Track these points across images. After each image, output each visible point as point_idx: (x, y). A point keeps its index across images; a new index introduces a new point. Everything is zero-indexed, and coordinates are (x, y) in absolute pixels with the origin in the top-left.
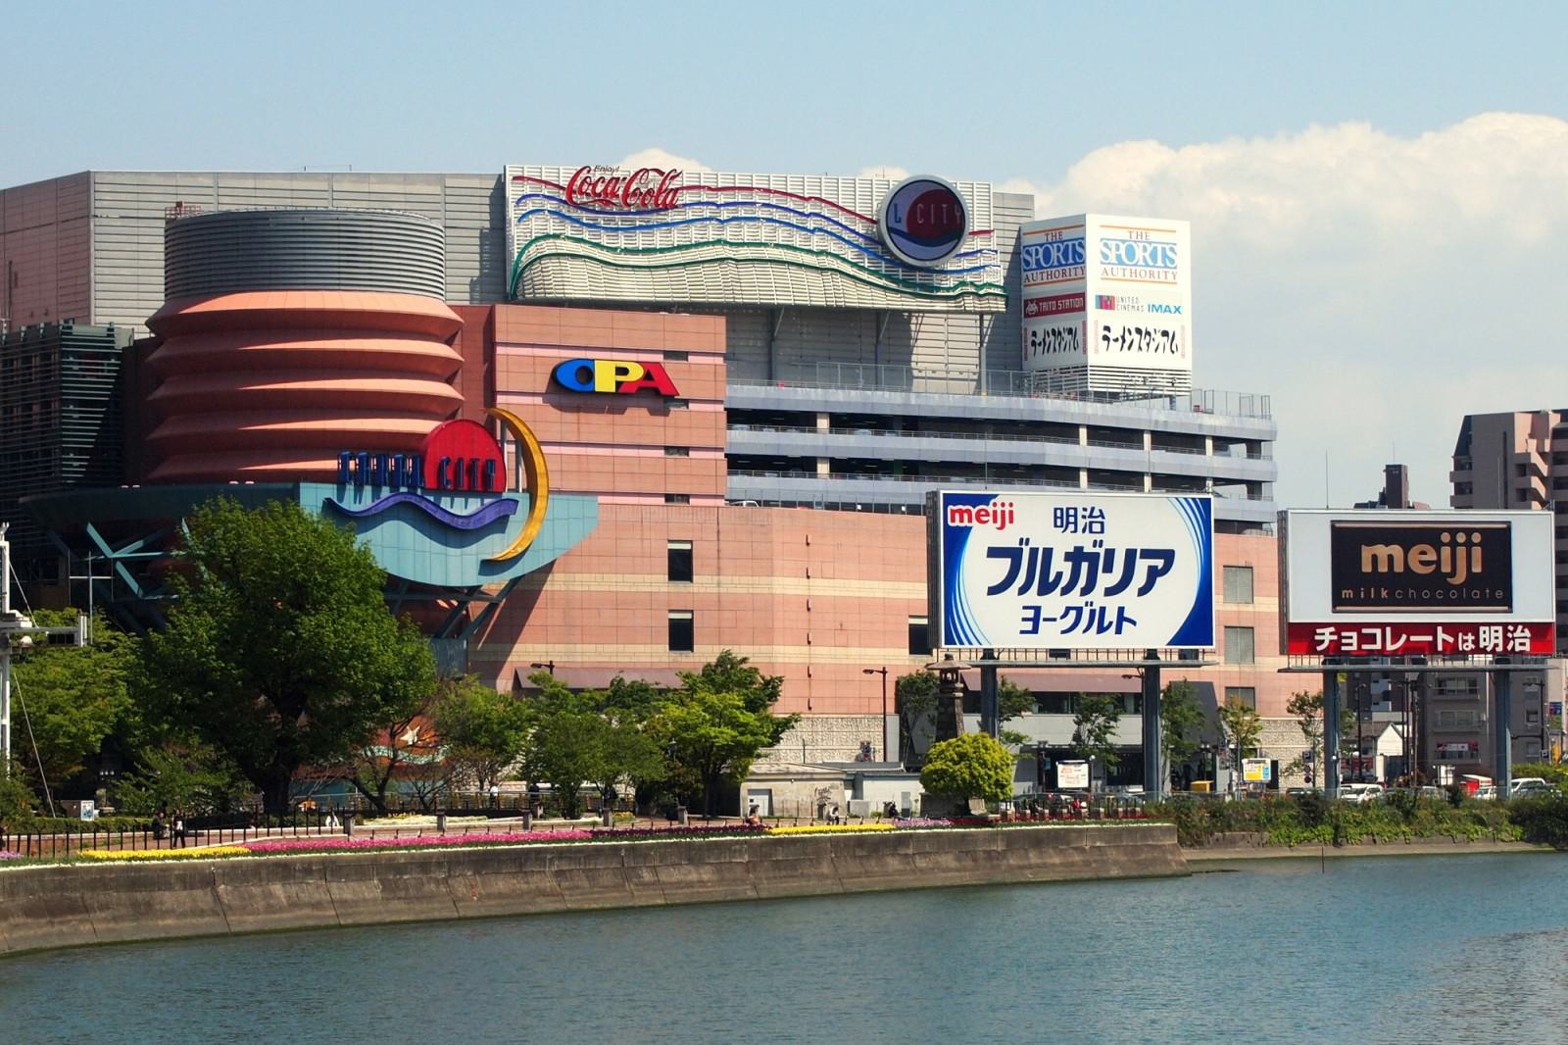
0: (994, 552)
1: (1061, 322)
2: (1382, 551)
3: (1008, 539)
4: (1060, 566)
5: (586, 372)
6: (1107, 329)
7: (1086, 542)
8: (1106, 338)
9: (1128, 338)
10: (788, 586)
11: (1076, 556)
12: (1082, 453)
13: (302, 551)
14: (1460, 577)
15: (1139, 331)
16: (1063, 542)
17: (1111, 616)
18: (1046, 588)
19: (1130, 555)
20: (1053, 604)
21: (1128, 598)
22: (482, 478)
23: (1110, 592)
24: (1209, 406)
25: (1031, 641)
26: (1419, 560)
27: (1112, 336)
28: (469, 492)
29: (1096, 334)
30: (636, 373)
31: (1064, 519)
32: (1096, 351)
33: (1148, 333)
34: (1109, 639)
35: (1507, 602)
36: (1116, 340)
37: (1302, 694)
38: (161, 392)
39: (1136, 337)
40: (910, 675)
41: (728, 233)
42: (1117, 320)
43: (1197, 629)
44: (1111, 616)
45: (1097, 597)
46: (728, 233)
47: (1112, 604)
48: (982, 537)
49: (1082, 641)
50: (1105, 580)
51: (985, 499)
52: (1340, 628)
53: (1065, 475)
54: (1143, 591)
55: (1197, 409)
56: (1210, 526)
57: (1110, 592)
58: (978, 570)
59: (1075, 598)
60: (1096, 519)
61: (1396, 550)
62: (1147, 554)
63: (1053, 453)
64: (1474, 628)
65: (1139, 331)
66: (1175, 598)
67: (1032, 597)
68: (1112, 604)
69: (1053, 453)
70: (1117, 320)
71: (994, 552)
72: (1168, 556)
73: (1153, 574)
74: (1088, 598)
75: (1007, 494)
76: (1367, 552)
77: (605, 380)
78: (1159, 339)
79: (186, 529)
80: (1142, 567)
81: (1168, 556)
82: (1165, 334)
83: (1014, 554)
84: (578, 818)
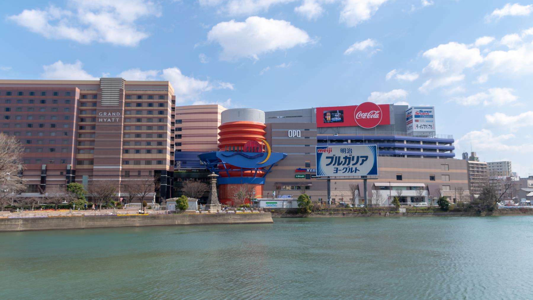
0: (327, 158)
1: (410, 125)
6: (417, 125)
8: (417, 127)
9: (422, 127)
15: (424, 125)
19: (358, 157)
20: (341, 167)
21: (358, 166)
27: (418, 126)
29: (415, 126)
31: (343, 151)
32: (415, 129)
33: (426, 125)
36: (419, 127)
39: (424, 126)
42: (419, 124)
45: (351, 166)
47: (354, 168)
48: (325, 155)
50: (352, 162)
54: (361, 164)
58: (324, 161)
60: (350, 151)
65: (424, 125)
70: (419, 124)
71: (327, 158)
72: (367, 157)
73: (363, 161)
78: (428, 126)
81: (367, 157)
82: (430, 125)
83: (332, 158)
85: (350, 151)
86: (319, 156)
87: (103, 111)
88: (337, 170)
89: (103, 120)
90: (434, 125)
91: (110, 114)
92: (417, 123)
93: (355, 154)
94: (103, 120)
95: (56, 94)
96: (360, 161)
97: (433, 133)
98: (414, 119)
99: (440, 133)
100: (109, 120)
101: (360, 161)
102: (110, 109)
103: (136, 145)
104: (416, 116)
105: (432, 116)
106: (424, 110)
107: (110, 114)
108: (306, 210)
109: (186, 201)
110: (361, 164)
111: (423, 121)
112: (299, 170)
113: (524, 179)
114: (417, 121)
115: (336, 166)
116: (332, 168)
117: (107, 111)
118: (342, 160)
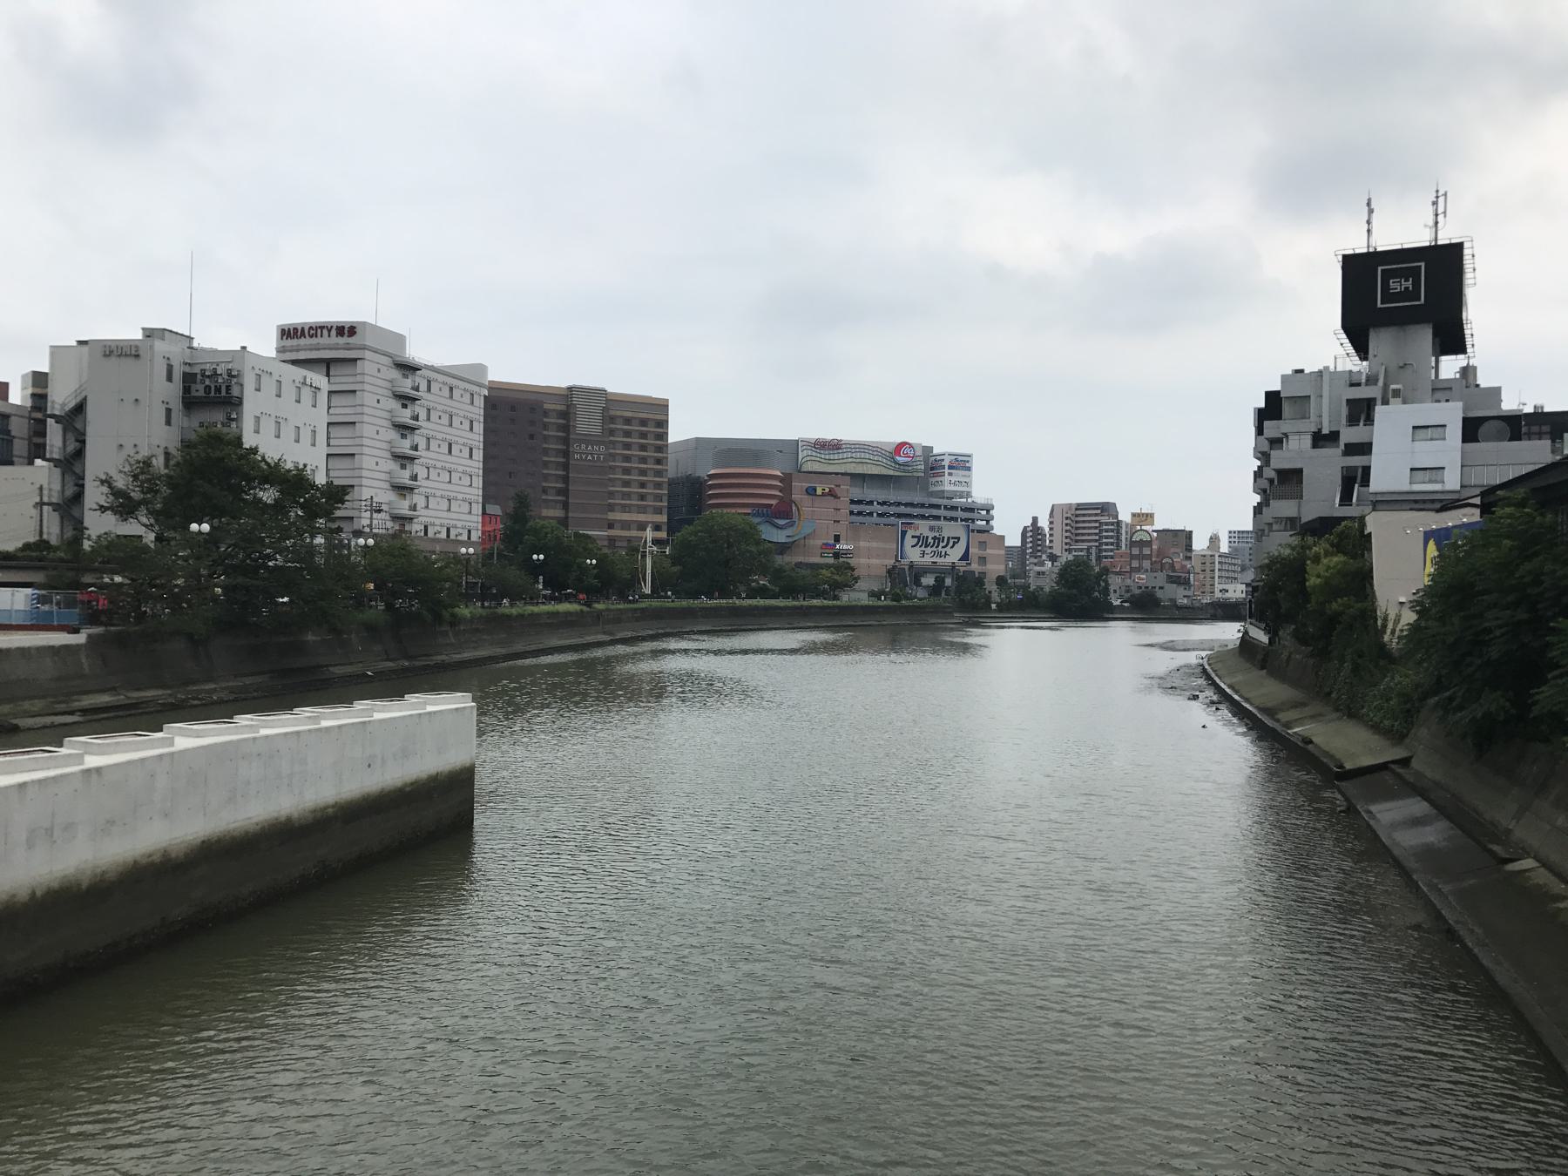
0: (913, 537)
1: (939, 479)
5: (815, 489)
12: (942, 512)
13: (495, 706)
19: (949, 538)
20: (929, 550)
21: (948, 549)
22: (787, 514)
24: (1417, 438)
25: (923, 559)
28: (784, 518)
30: (827, 490)
31: (932, 529)
34: (942, 559)
37: (301, 466)
41: (854, 455)
42: (953, 479)
43: (965, 557)
45: (940, 549)
46: (854, 455)
47: (943, 551)
48: (910, 533)
50: (942, 544)
53: (937, 518)
54: (952, 547)
56: (969, 530)
58: (909, 541)
60: (940, 529)
63: (935, 512)
68: (943, 551)
69: (935, 512)
70: (953, 479)
71: (913, 537)
72: (959, 539)
73: (954, 543)
75: (916, 522)
77: (819, 491)
79: (1471, 882)
81: (959, 539)
83: (919, 537)
85: (940, 529)
86: (904, 533)
87: (581, 442)
88: (924, 554)
89: (581, 457)
90: (971, 481)
91: (590, 448)
92: (950, 478)
93: (946, 534)
94: (581, 457)
95: (513, 409)
96: (951, 544)
97: (969, 495)
98: (947, 471)
99: (979, 495)
100: (590, 457)
101: (951, 544)
102: (588, 440)
103: (623, 499)
104: (950, 467)
105: (969, 469)
106: (960, 458)
107: (590, 448)
108: (959, 591)
109: (1177, 566)
110: (952, 547)
111: (958, 475)
112: (826, 546)
113: (123, 540)
114: (950, 474)
115: (923, 548)
116: (918, 550)
117: (587, 443)
118: (930, 540)
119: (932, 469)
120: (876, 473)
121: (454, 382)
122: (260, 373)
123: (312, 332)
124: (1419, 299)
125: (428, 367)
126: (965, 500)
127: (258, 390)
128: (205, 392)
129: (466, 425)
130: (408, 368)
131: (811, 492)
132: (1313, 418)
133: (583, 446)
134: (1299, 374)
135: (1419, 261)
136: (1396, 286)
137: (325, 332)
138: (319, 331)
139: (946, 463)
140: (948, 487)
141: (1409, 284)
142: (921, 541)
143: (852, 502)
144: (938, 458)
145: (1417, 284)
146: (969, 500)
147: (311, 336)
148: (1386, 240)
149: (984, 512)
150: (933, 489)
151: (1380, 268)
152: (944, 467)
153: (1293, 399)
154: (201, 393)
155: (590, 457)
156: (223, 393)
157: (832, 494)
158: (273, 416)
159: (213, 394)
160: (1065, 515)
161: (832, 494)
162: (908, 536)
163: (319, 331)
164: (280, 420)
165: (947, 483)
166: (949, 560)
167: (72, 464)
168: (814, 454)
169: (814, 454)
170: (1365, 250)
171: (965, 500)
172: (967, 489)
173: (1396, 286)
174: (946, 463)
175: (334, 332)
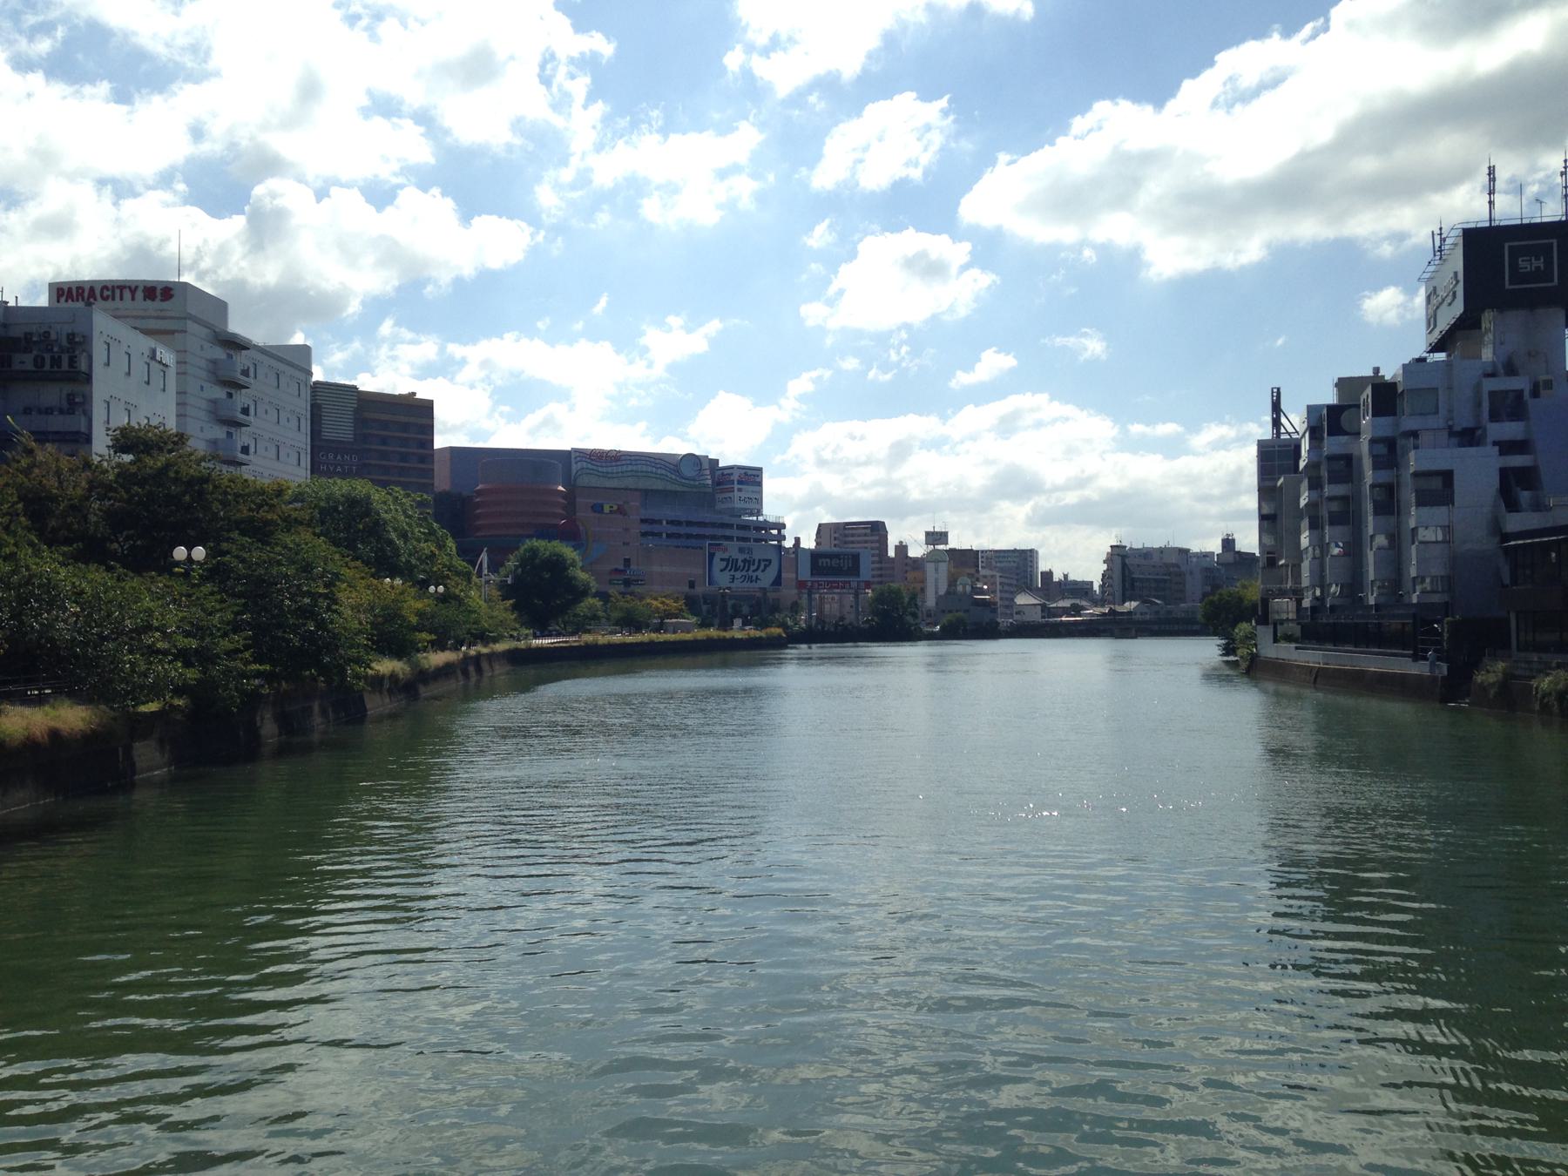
0: (722, 560)
1: (727, 495)
2: (824, 560)
3: (726, 556)
4: (740, 563)
7: (747, 556)
10: (656, 569)
11: (744, 561)
14: (846, 568)
16: (741, 557)
17: (754, 578)
18: (736, 570)
19: (759, 561)
20: (738, 574)
21: (759, 573)
23: (754, 571)
26: (835, 562)
30: (615, 508)
31: (741, 550)
35: (858, 575)
38: (478, 511)
40: (998, 352)
42: (743, 495)
43: (778, 581)
44: (754, 578)
45: (750, 573)
48: (719, 555)
49: (746, 584)
50: (752, 568)
51: (719, 545)
52: (812, 582)
55: (422, 1053)
57: (754, 571)
58: (718, 565)
59: (744, 573)
60: (750, 551)
61: (828, 560)
62: (764, 560)
64: (849, 582)
66: (771, 573)
67: (732, 573)
68: (755, 574)
70: (743, 495)
71: (722, 560)
72: (770, 561)
73: (766, 566)
74: (756, 574)
76: (820, 561)
77: (607, 509)
80: (763, 564)
81: (770, 561)
84: (1283, 257)
86: (712, 556)
91: (339, 457)
92: (740, 494)
96: (762, 567)
98: (736, 486)
101: (762, 567)
107: (339, 457)
110: (763, 571)
111: (748, 490)
114: (740, 490)
116: (727, 575)
119: (719, 484)
120: (660, 488)
121: (282, 367)
122: (109, 340)
123: (106, 293)
124: (1552, 281)
125: (256, 347)
126: (755, 518)
127: (108, 364)
128: (36, 366)
129: (294, 423)
130: (235, 344)
131: (597, 508)
132: (1443, 412)
133: (331, 456)
134: (1420, 364)
135: (1552, 238)
136: (1525, 265)
137: (127, 294)
138: (118, 292)
139: (735, 477)
140: (738, 505)
141: (1541, 263)
142: (731, 564)
143: (643, 521)
144: (726, 472)
145: (1549, 263)
146: (761, 519)
147: (105, 299)
148: (1509, 210)
149: (775, 532)
150: (720, 506)
151: (1507, 245)
152: (732, 482)
153: (1415, 392)
154: (30, 366)
155: (339, 469)
156: (65, 366)
157: (621, 511)
158: (123, 401)
159: (47, 367)
160: (834, 535)
161: (621, 511)
162: (716, 560)
163: (118, 292)
164: (129, 407)
165: (736, 499)
166: (760, 584)
167: (687, 434)
168: (589, 466)
169: (589, 466)
170: (1487, 224)
171: (755, 518)
172: (757, 507)
173: (1525, 265)
174: (735, 477)
175: (140, 295)
